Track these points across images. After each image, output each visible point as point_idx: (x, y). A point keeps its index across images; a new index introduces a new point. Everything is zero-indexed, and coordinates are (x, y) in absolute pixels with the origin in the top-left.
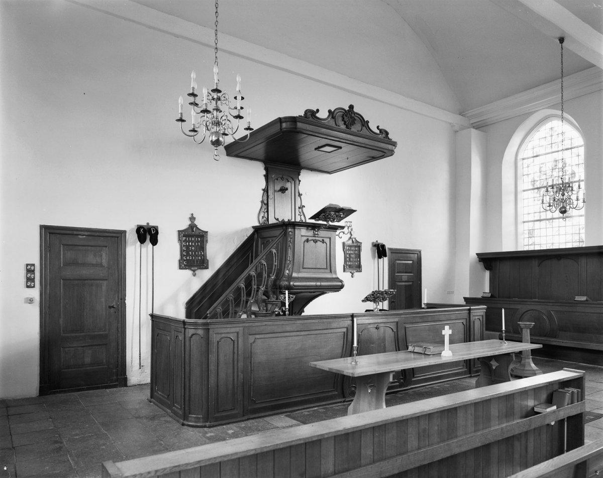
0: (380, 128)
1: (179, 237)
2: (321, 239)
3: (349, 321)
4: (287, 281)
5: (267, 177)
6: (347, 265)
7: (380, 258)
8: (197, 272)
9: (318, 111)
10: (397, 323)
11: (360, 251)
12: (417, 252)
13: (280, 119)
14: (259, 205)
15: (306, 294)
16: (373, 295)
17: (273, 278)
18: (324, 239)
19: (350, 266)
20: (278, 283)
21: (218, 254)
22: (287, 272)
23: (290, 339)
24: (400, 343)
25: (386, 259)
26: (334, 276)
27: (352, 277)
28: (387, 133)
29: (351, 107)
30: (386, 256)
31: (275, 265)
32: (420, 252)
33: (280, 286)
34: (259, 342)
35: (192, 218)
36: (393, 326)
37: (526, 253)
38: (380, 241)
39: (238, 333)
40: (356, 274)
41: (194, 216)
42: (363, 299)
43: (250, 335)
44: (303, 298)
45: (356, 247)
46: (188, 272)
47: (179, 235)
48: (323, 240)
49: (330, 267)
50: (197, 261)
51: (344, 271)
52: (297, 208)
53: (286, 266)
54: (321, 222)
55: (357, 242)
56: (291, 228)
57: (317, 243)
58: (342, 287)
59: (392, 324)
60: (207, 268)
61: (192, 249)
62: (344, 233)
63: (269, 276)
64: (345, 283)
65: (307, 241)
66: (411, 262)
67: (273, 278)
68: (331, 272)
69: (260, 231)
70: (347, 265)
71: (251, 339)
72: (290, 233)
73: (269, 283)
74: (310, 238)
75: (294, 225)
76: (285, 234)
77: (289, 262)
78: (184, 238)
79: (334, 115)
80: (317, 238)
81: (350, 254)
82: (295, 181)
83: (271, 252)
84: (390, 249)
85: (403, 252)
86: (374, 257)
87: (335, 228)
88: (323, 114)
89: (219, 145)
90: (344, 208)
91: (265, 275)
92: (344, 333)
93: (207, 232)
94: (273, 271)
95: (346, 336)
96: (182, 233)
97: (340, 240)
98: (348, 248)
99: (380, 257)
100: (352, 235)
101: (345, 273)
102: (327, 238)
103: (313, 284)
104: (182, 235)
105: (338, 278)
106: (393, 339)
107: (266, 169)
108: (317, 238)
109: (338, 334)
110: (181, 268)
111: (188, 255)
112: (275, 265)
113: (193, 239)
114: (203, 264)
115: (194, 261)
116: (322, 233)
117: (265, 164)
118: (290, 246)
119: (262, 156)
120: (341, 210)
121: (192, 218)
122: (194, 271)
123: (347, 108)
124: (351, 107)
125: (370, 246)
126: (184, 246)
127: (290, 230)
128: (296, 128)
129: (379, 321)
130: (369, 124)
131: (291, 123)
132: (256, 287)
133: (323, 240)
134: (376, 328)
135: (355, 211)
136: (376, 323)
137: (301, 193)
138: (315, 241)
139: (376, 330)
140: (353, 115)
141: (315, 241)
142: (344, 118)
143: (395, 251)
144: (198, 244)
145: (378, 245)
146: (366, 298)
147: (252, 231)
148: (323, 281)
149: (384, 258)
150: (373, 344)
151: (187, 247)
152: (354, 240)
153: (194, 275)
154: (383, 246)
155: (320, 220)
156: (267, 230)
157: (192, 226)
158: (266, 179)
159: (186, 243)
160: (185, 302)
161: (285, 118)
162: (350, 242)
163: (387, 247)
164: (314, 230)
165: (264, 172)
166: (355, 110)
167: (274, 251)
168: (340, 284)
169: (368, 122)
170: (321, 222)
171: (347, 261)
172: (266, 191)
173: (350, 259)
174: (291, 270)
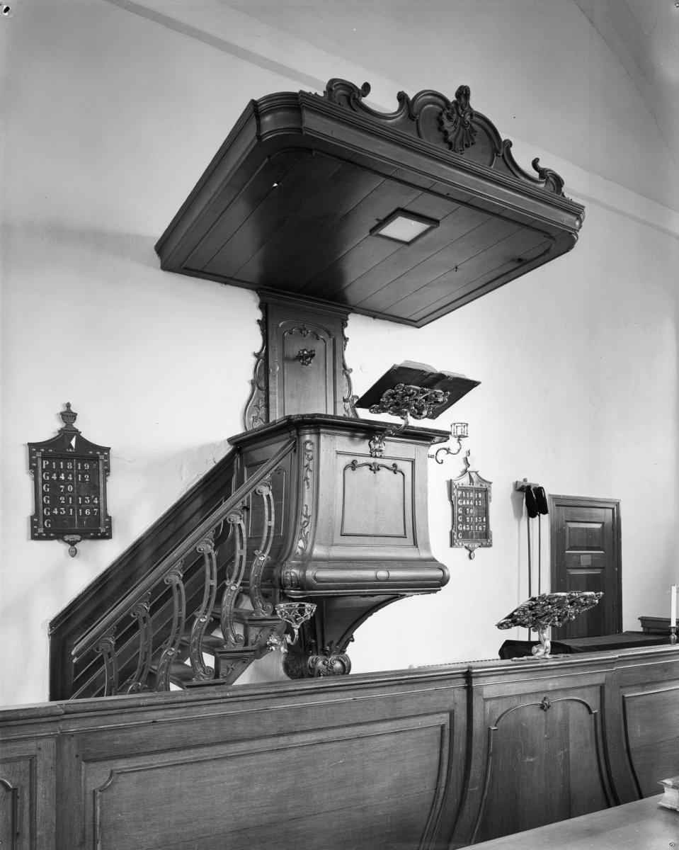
0: (541, 165)
1: (31, 461)
2: (389, 463)
3: (456, 692)
4: (297, 566)
5: (264, 325)
6: (458, 531)
7: (533, 516)
8: (79, 546)
9: (367, 87)
10: (602, 688)
11: (486, 499)
12: (612, 506)
13: (254, 104)
14: (247, 390)
15: (354, 600)
16: (531, 608)
17: (262, 559)
18: (398, 462)
19: (465, 535)
20: (275, 572)
21: (136, 505)
22: (301, 544)
23: (253, 762)
24: (610, 748)
25: (545, 519)
26: (424, 555)
27: (471, 558)
28: (558, 183)
29: (463, 93)
30: (545, 512)
31: (270, 527)
32: (618, 505)
33: (280, 580)
34: (128, 786)
35: (68, 415)
36: (592, 699)
37: (618, 553)
38: (534, 480)
39: (32, 760)
40: (479, 552)
41: (73, 409)
42: (501, 619)
43: (87, 761)
44: (331, 617)
45: (478, 491)
46: (57, 548)
47: (31, 454)
48: (395, 465)
49: (413, 532)
50: (80, 520)
51: (452, 545)
52: (339, 399)
53: (299, 527)
54: (385, 417)
55: (482, 480)
56: (310, 434)
57: (378, 472)
58: (443, 581)
59: (586, 690)
60: (107, 536)
61: (66, 489)
62: (448, 450)
63: (251, 556)
64: (451, 572)
65: (353, 466)
66: (599, 526)
67: (262, 559)
68: (415, 544)
69: (248, 448)
70: (458, 531)
71: (96, 776)
72: (308, 447)
73: (254, 573)
74: (361, 460)
75: (318, 424)
76: (296, 448)
77: (304, 519)
78: (46, 463)
79: (415, 110)
80: (379, 461)
81: (464, 508)
82: (334, 340)
83: (257, 496)
84: (555, 498)
85: (582, 504)
86: (518, 515)
87: (425, 437)
88: (382, 101)
89: (663, 791)
90: (446, 374)
91: (241, 552)
92: (443, 727)
93: (108, 449)
94: (264, 542)
95: (447, 740)
96: (38, 450)
97: (439, 472)
98: (460, 493)
99: (532, 514)
100: (469, 465)
101: (453, 549)
102: (407, 460)
103: (370, 574)
104: (39, 455)
105: (433, 560)
106: (588, 735)
107: (263, 307)
108: (379, 461)
109: (422, 733)
110: (35, 536)
111: (55, 502)
112: (270, 527)
113: (70, 466)
114: (97, 527)
115: (72, 520)
116: (392, 448)
117: (260, 295)
118: (307, 479)
119: (253, 269)
120: (439, 380)
121: (68, 415)
122: (72, 543)
123: (452, 98)
124: (463, 93)
125: (510, 490)
126: (44, 482)
127: (308, 437)
128: (300, 130)
129: (550, 685)
130: (512, 150)
131: (287, 113)
132: (214, 583)
133: (395, 465)
134: (542, 707)
135: (471, 385)
136: (542, 692)
137: (349, 366)
138: (374, 468)
139: (542, 712)
140: (468, 117)
141: (374, 468)
142: (441, 123)
143: (562, 502)
144: (83, 478)
145: (529, 487)
146: (511, 616)
147: (227, 449)
148: (393, 569)
149: (541, 515)
150: (532, 755)
151: (54, 485)
152: (473, 475)
153: (74, 553)
154: (539, 491)
155: (384, 410)
156: (260, 444)
157: (68, 431)
158: (262, 330)
159: (51, 476)
160: (49, 622)
161: (270, 98)
162: (465, 481)
163: (549, 492)
164: (371, 439)
165: (259, 315)
166: (476, 104)
167: (266, 491)
168: (440, 573)
169: (509, 144)
170: (385, 417)
171: (459, 523)
172: (263, 359)
173: (464, 519)
174: (310, 540)
